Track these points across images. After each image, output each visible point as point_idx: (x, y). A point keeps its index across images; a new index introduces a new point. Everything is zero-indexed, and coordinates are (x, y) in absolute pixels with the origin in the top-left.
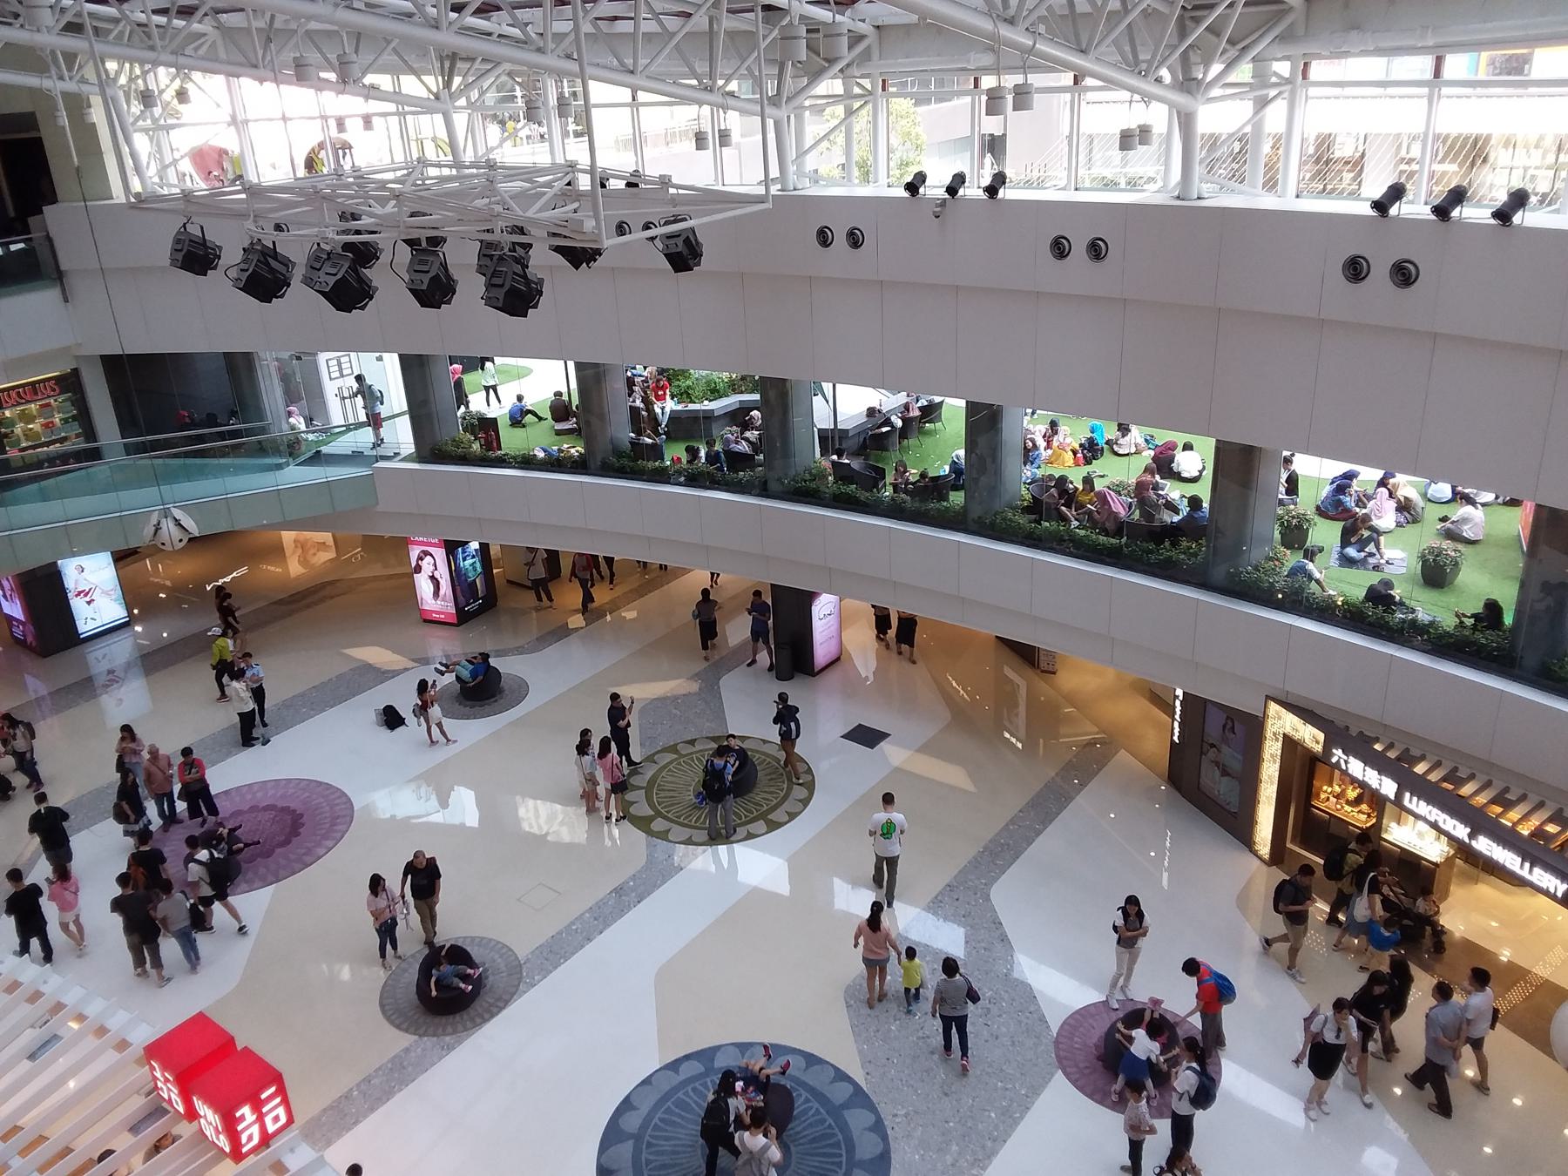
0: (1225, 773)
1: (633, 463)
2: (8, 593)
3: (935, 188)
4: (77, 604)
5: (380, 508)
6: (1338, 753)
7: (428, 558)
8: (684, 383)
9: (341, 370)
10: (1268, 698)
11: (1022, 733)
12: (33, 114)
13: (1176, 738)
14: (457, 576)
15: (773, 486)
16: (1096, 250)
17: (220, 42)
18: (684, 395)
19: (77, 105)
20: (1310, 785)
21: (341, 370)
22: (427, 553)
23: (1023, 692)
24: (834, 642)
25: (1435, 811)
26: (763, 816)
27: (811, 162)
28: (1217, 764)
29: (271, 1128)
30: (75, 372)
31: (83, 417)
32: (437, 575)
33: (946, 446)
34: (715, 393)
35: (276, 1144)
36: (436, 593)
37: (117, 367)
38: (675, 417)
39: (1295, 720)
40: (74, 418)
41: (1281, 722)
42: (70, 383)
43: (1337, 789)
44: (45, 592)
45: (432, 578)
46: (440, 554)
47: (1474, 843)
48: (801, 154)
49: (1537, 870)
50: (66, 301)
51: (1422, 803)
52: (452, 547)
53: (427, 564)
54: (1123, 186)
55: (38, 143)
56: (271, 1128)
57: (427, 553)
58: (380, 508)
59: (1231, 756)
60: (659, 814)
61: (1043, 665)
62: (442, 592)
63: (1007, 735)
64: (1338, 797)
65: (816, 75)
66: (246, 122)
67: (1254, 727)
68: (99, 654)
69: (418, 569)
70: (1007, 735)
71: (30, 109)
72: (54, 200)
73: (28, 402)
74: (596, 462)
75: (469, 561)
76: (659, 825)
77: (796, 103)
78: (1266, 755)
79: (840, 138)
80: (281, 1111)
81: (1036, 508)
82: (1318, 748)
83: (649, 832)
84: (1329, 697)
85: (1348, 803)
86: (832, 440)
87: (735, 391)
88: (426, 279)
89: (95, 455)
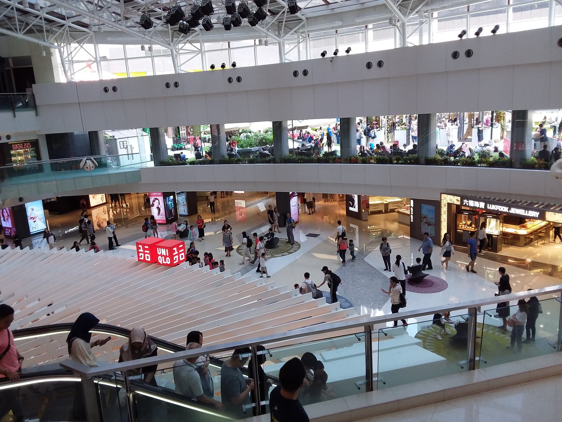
0: (429, 225)
1: (231, 159)
2: (6, 218)
3: (330, 55)
4: (30, 222)
6: (465, 201)
7: (157, 201)
8: (240, 144)
9: (123, 144)
10: (441, 193)
13: (412, 221)
14: (166, 207)
15: (278, 160)
16: (380, 64)
17: (94, 36)
20: (456, 224)
21: (123, 144)
22: (156, 199)
25: (497, 206)
28: (426, 223)
31: (39, 157)
32: (159, 206)
36: (159, 213)
37: (50, 138)
38: (239, 152)
39: (451, 197)
40: (35, 157)
41: (446, 199)
42: (35, 144)
43: (464, 222)
44: (20, 215)
46: (161, 199)
47: (510, 211)
49: (530, 212)
50: (37, 115)
51: (493, 206)
52: (166, 195)
56: (181, 259)
57: (156, 199)
59: (431, 216)
61: (364, 218)
62: (161, 212)
64: (465, 225)
67: (437, 204)
68: (36, 241)
69: (153, 205)
71: (26, 54)
72: (35, 83)
73: (21, 149)
75: (170, 203)
78: (442, 213)
79: (296, 49)
82: (459, 203)
84: (461, 186)
85: (468, 226)
86: (291, 151)
87: (257, 146)
89: (40, 169)
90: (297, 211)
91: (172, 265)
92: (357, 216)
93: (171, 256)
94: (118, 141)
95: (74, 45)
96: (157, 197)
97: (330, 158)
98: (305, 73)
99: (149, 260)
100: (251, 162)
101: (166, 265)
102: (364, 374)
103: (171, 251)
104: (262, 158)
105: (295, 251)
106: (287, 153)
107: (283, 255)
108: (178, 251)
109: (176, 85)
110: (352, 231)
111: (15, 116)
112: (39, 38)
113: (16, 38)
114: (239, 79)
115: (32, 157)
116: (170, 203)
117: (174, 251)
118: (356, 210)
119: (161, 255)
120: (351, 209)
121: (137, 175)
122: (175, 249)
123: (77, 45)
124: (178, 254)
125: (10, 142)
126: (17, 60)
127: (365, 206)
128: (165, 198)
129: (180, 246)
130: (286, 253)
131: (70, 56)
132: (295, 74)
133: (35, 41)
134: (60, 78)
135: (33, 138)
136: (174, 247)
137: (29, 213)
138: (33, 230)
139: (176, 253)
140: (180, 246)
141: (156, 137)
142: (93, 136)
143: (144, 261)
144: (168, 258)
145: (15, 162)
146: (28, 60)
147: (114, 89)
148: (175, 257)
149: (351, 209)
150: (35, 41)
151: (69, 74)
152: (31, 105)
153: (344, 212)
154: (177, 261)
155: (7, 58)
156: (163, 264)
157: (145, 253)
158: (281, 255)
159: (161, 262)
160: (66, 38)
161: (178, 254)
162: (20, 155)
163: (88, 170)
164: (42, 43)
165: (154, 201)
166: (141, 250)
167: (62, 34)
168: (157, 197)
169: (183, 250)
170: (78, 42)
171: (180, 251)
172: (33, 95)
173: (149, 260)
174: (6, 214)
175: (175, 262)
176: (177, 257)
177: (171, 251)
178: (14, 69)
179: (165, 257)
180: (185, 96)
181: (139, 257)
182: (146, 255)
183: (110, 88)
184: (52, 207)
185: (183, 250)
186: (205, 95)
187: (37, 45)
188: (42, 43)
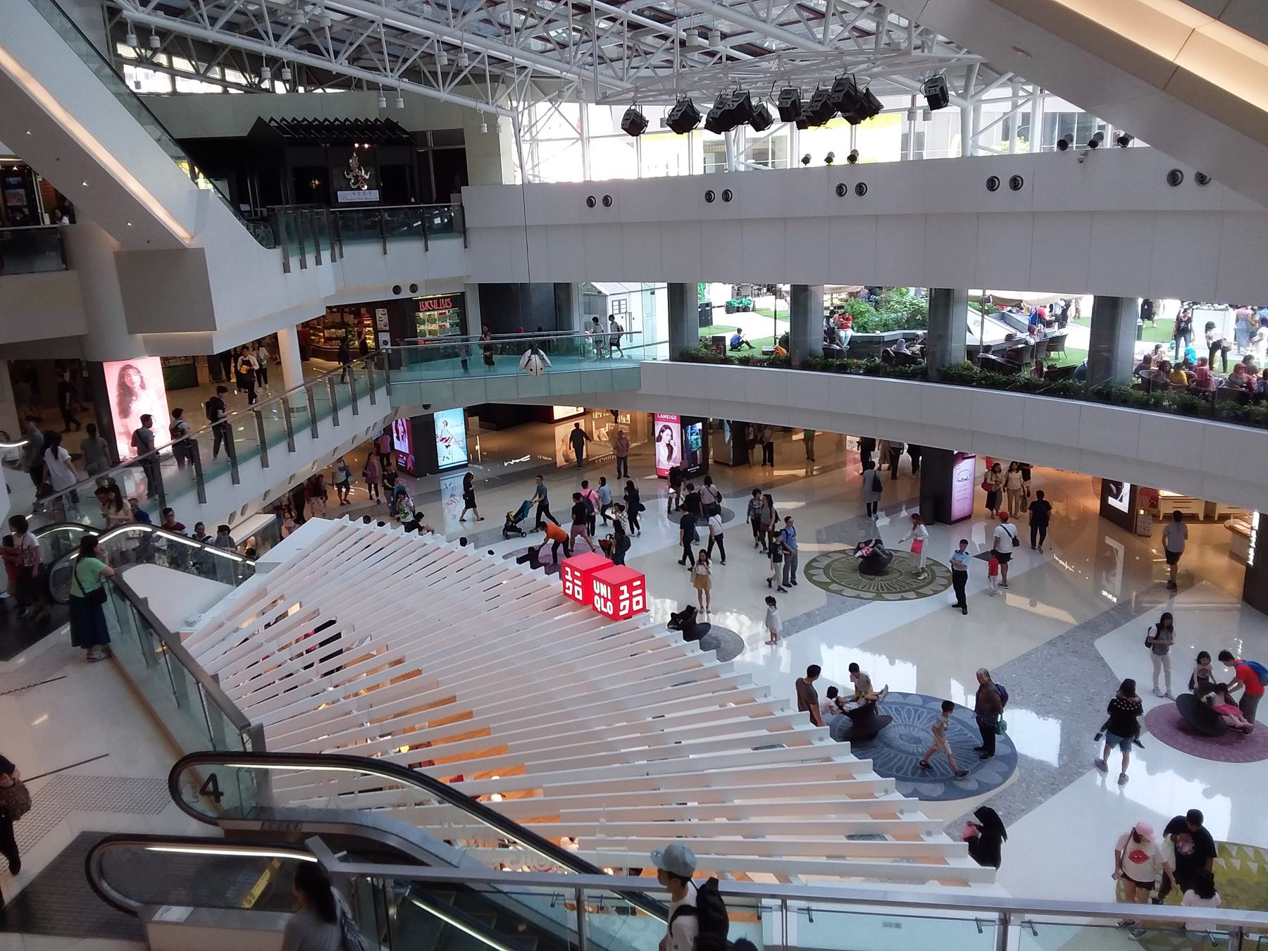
1: (830, 361)
4: (440, 446)
5: (642, 391)
7: (668, 431)
8: (861, 321)
11: (1118, 592)
12: (461, 132)
14: (685, 445)
18: (863, 328)
19: (492, 120)
23: (1121, 554)
24: (968, 502)
26: (913, 590)
27: (982, 140)
29: (635, 608)
30: (463, 294)
31: (463, 326)
33: (1077, 343)
34: (886, 327)
35: (635, 617)
37: (487, 291)
38: (853, 341)
40: (457, 324)
42: (458, 301)
45: (668, 445)
46: (676, 428)
48: (976, 134)
52: (686, 422)
53: (666, 436)
54: (1201, 518)
55: (464, 150)
56: (635, 608)
57: (667, 427)
58: (642, 391)
60: (834, 582)
63: (1105, 593)
65: (988, 84)
66: (589, 138)
69: (660, 439)
70: (1105, 593)
74: (795, 362)
75: (694, 437)
76: (834, 587)
77: (977, 98)
80: (640, 598)
81: (1148, 385)
83: (828, 590)
86: (971, 352)
87: (900, 328)
88: (790, 102)
90: (969, 491)
91: (616, 617)
92: (1124, 522)
93: (616, 602)
94: (610, 299)
95: (543, 107)
96: (670, 424)
97: (1060, 383)
98: (1016, 183)
99: (580, 597)
100: (871, 371)
101: (607, 614)
102: (1010, 927)
103: (616, 592)
104: (896, 365)
105: (936, 592)
106: (958, 357)
107: (903, 599)
108: (630, 591)
109: (726, 196)
110: (1108, 554)
111: (427, 250)
112: (476, 97)
113: (437, 100)
114: (861, 190)
115: (452, 325)
116: (694, 437)
117: (622, 592)
118: (1122, 505)
119: (599, 595)
120: (1112, 501)
121: (639, 372)
122: (624, 588)
123: (549, 105)
124: (630, 598)
125: (418, 296)
126: (440, 135)
127: (1146, 500)
128: (684, 427)
129: (635, 584)
130: (912, 594)
131: (534, 129)
132: (992, 184)
133: (470, 103)
134: (511, 175)
135: (457, 290)
136: (622, 584)
137: (440, 430)
138: (443, 462)
139: (626, 595)
140: (635, 584)
141: (679, 297)
142: (562, 292)
143: (572, 597)
144: (609, 604)
145: (423, 334)
146: (457, 136)
147: (607, 201)
148: (622, 604)
149: (1112, 501)
150: (470, 103)
151: (528, 167)
152: (456, 227)
153: (1094, 504)
154: (626, 611)
155: (424, 133)
156: (602, 612)
157: (574, 584)
158: (899, 596)
159: (598, 606)
160: (529, 93)
161: (630, 598)
162: (434, 321)
163: (533, 373)
164: (482, 107)
165: (662, 431)
166: (569, 577)
167: (522, 83)
168: (670, 424)
169: (640, 591)
170: (550, 101)
171: (634, 593)
172: (462, 206)
173: (580, 597)
174: (401, 429)
175: (621, 613)
176: (627, 603)
177: (616, 592)
178: (434, 151)
179: (606, 600)
180: (742, 221)
181: (565, 588)
182: (577, 588)
183: (599, 198)
184: (488, 418)
185: (640, 591)
186: (785, 220)
187: (474, 110)
188: (482, 107)
